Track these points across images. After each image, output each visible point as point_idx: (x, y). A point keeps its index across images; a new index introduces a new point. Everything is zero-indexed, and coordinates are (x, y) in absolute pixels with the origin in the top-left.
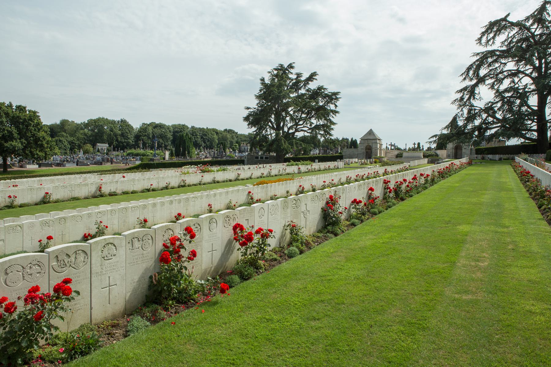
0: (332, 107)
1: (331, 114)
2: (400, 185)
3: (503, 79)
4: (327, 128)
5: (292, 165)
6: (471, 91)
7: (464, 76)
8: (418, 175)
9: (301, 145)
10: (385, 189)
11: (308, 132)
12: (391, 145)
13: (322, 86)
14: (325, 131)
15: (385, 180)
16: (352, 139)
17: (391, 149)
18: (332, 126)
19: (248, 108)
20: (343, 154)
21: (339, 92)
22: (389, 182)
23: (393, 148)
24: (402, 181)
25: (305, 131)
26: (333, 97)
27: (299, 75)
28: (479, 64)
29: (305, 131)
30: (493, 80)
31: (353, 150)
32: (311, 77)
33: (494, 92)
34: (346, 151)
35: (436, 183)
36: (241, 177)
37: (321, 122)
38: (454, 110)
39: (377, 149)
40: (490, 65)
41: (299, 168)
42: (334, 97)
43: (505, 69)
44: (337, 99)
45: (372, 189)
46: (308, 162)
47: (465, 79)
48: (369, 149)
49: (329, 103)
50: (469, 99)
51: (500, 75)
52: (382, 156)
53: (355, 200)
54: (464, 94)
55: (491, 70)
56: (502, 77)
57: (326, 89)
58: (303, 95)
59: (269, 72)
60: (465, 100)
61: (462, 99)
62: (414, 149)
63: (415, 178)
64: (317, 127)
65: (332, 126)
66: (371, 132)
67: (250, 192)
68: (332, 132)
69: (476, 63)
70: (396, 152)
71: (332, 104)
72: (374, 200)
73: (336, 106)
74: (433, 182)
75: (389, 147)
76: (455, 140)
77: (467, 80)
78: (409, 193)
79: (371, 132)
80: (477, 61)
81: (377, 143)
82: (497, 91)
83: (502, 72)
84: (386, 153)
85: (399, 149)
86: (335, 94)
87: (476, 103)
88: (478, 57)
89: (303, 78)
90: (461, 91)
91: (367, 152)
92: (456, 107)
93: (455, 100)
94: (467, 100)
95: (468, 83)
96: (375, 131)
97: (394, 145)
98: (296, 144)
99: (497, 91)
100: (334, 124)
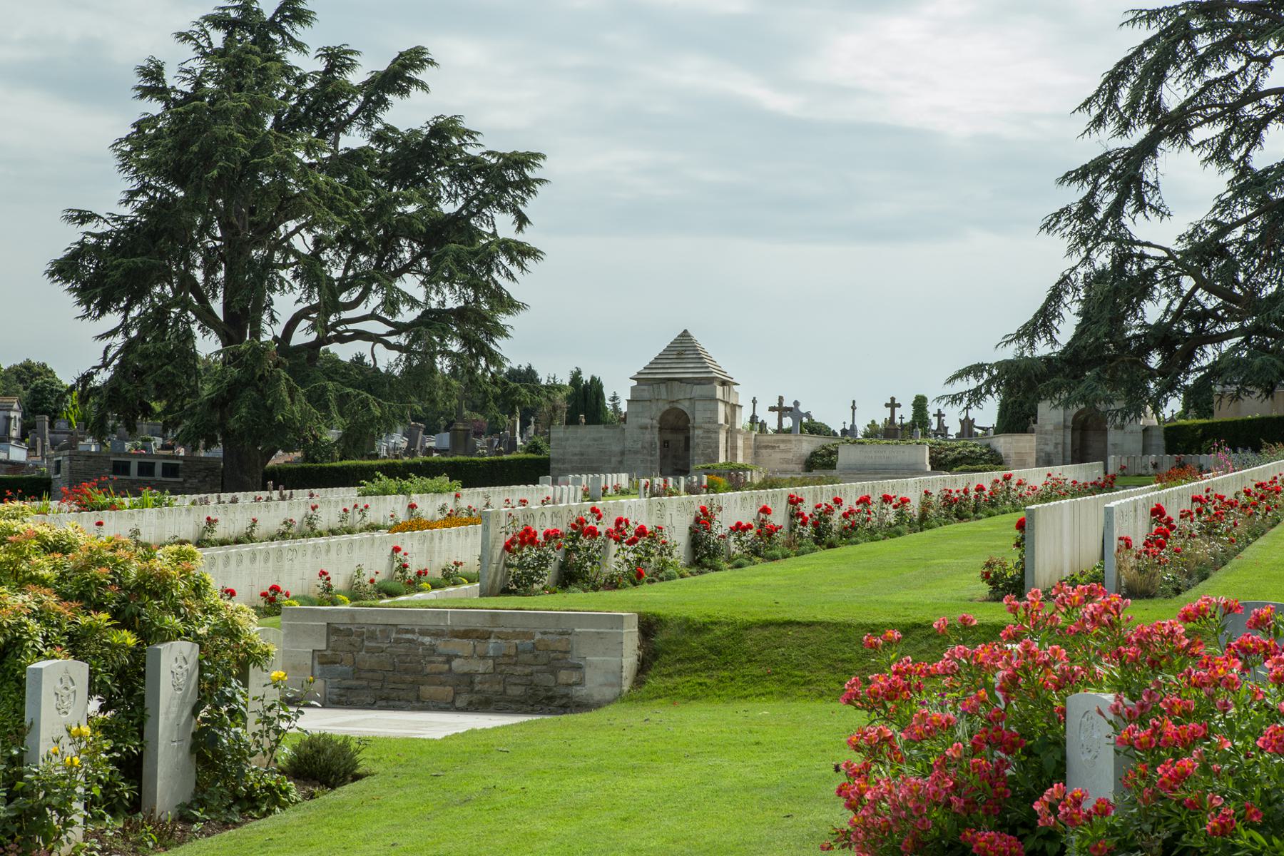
0: (504, 225)
1: (504, 260)
2: (825, 512)
3: (1263, 123)
4: (478, 324)
5: (385, 492)
6: (1128, 176)
7: (1095, 111)
8: (876, 498)
9: (365, 404)
10: (792, 517)
11: (389, 346)
12: (781, 410)
13: (452, 120)
14: (467, 340)
15: (791, 496)
16: (576, 378)
17: (780, 430)
18: (503, 319)
19: (84, 217)
20: (551, 452)
21: (537, 156)
22: (801, 500)
23: (788, 422)
24: (831, 502)
25: (375, 338)
26: (508, 177)
27: (337, 59)
28: (1155, 61)
29: (375, 338)
30: (1220, 128)
31: (585, 434)
32: (400, 75)
33: (1231, 174)
34: (566, 439)
35: (930, 528)
36: (220, 532)
37: (450, 298)
38: (1054, 257)
39: (712, 432)
40: (1201, 64)
41: (412, 507)
42: (512, 175)
43: (1267, 84)
44: (526, 185)
45: (765, 510)
46: (444, 480)
47: (1099, 121)
48: (675, 429)
49: (486, 203)
50: (1116, 210)
51: (1248, 108)
52: (740, 460)
53: (739, 524)
54: (1096, 187)
55: (1209, 85)
56: (1258, 114)
57: (470, 134)
58: (355, 156)
59: (185, 37)
60: (1100, 216)
61: (1088, 207)
62: (891, 432)
63: (865, 501)
64: (433, 320)
65: (503, 319)
66: (683, 347)
67: (397, 549)
68: (501, 346)
69: (1149, 56)
70: (808, 445)
71: (503, 208)
72: (773, 530)
73: (522, 220)
74: (923, 522)
75: (772, 421)
76: (1058, 388)
77: (1111, 126)
78: (849, 533)
79: (683, 347)
80: (1148, 44)
81: (714, 400)
82: (1243, 168)
83: (1253, 95)
84: (757, 449)
85: (815, 429)
86: (520, 161)
87: (1140, 226)
88: (1154, 30)
89: (356, 77)
90: (1082, 174)
91: (665, 444)
92: (1065, 243)
93: (1057, 215)
94: (1107, 216)
95: (1109, 140)
96: (703, 340)
97: (793, 411)
98: (342, 399)
99: (1243, 168)
100: (510, 305)
